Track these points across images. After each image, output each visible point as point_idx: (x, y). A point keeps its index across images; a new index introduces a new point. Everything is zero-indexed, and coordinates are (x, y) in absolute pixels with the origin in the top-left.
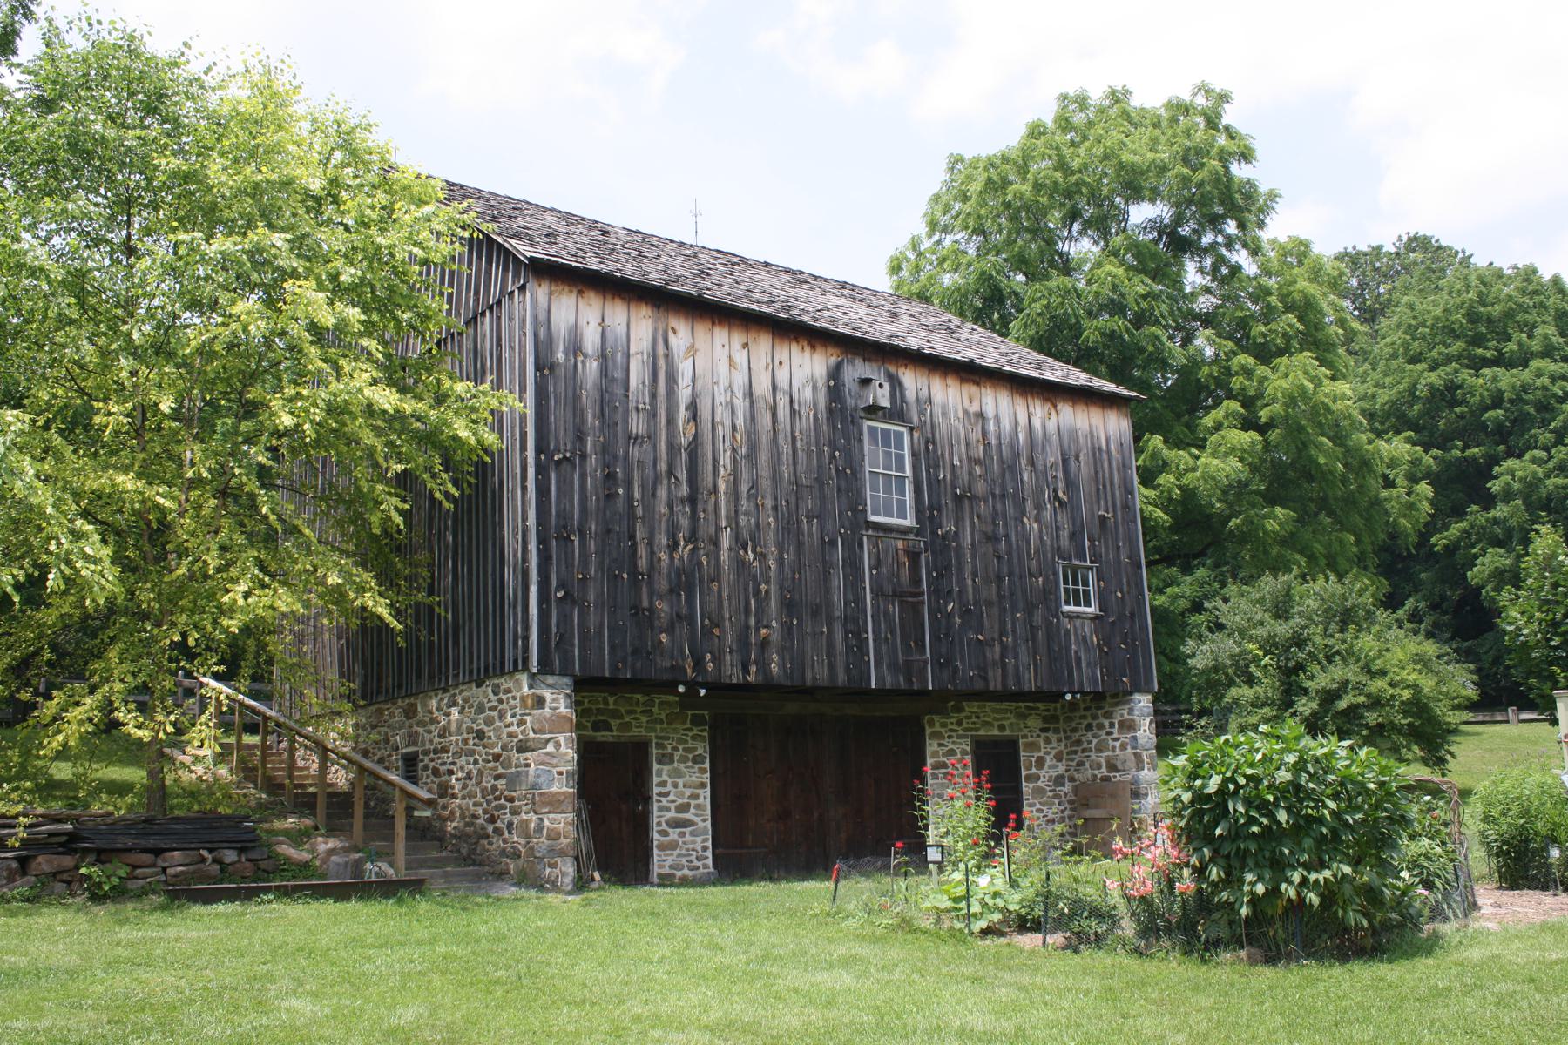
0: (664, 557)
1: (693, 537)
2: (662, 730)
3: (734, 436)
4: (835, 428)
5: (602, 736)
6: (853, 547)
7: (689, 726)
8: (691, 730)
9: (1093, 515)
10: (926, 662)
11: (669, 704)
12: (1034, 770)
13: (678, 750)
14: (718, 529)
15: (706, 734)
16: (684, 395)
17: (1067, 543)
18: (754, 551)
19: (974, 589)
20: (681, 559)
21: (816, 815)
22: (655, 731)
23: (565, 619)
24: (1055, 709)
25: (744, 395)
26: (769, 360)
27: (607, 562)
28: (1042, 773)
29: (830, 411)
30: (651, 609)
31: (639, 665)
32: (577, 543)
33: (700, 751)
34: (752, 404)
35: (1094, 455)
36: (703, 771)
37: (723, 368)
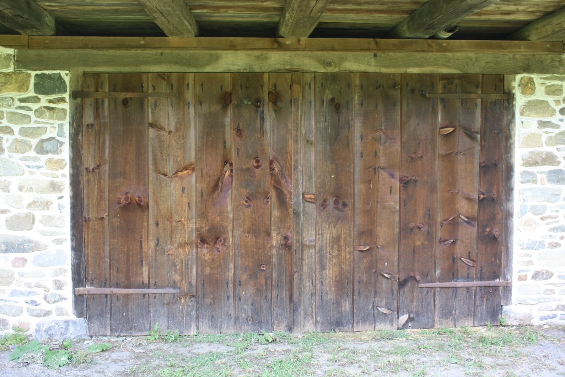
7: (31, 93)
21: (276, 239)
33: (51, 132)
36: (59, 164)
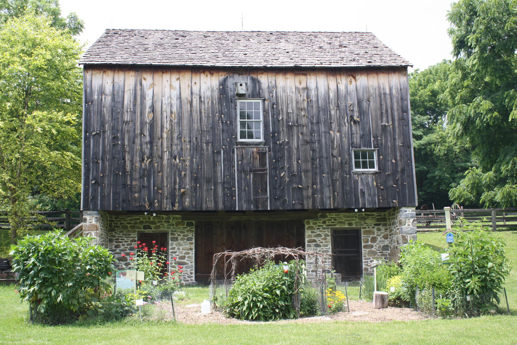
0: (138, 165)
1: (151, 156)
2: (173, 228)
3: (171, 116)
4: (222, 105)
5: (147, 231)
6: (229, 153)
8: (186, 228)
9: (377, 125)
10: (267, 198)
11: (177, 218)
12: (370, 243)
13: (180, 235)
14: (163, 152)
15: (194, 229)
16: (148, 103)
17: (358, 140)
18: (180, 160)
19: (297, 165)
20: (146, 165)
22: (170, 228)
23: (95, 191)
24: (385, 215)
25: (177, 99)
26: (190, 83)
27: (113, 169)
28: (375, 244)
29: (220, 99)
30: (131, 185)
31: (125, 206)
32: (101, 164)
33: (190, 236)
34: (181, 102)
35: (380, 96)
37: (167, 90)
